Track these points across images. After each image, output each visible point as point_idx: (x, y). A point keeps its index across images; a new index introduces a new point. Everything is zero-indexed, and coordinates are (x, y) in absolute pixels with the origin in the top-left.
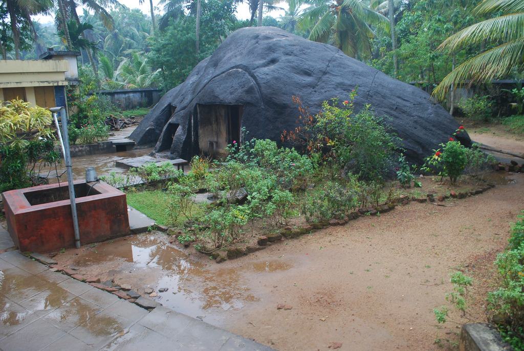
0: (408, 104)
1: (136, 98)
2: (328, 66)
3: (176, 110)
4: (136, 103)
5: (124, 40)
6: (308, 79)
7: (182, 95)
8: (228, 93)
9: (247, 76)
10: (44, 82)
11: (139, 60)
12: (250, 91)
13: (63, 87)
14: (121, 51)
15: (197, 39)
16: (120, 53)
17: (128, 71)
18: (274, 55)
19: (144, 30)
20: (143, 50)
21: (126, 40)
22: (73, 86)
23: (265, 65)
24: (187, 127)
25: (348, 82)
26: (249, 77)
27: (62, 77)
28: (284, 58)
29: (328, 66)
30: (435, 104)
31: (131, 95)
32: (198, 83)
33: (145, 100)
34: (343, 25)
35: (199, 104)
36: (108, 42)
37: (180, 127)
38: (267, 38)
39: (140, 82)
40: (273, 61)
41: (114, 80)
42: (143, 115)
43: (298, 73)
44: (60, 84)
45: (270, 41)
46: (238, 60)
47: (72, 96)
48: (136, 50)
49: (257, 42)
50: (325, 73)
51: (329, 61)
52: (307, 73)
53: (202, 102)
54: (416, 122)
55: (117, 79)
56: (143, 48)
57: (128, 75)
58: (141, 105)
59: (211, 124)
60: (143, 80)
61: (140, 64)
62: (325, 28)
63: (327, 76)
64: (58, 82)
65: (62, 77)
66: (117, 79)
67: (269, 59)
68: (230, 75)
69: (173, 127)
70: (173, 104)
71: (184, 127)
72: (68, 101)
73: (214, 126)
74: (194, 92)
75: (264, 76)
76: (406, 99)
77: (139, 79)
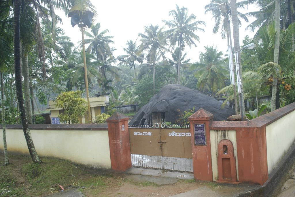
0: (217, 109)
1: (129, 108)
2: (192, 99)
3: (145, 114)
4: (129, 111)
5: (122, 80)
6: (185, 103)
7: (147, 108)
8: (161, 108)
9: (167, 103)
10: (97, 105)
11: (129, 91)
12: (167, 108)
13: (104, 106)
14: (120, 85)
15: (154, 83)
16: (120, 86)
17: (124, 96)
18: (175, 96)
19: (131, 76)
20: (130, 84)
21: (123, 80)
22: (108, 106)
23: (172, 99)
24: (148, 120)
25: (198, 104)
26: (167, 103)
27: (103, 103)
28: (178, 97)
29: (192, 99)
30: (228, 109)
31: (127, 107)
32: (152, 105)
33: (133, 109)
34: (211, 76)
35: (152, 112)
36: (114, 82)
37: (146, 120)
38: (174, 89)
39: (130, 101)
40: (175, 98)
41: (118, 100)
42: (132, 116)
43: (182, 101)
44: (103, 105)
45: (174, 91)
46: (165, 97)
47: (107, 109)
48: (127, 85)
49: (171, 91)
50: (191, 101)
51: (193, 97)
52: (185, 101)
53: (153, 111)
54: (219, 115)
55: (120, 100)
56: (131, 84)
57: (124, 98)
58: (131, 112)
59: (156, 118)
60: (131, 100)
61: (130, 93)
62: (204, 78)
63: (191, 102)
64: (102, 105)
65: (103, 103)
66: (120, 100)
67: (174, 97)
68: (162, 102)
69: (144, 120)
70: (144, 112)
71: (147, 120)
72: (106, 111)
73: (158, 119)
74: (151, 108)
75: (172, 103)
76: (217, 108)
77: (129, 99)
